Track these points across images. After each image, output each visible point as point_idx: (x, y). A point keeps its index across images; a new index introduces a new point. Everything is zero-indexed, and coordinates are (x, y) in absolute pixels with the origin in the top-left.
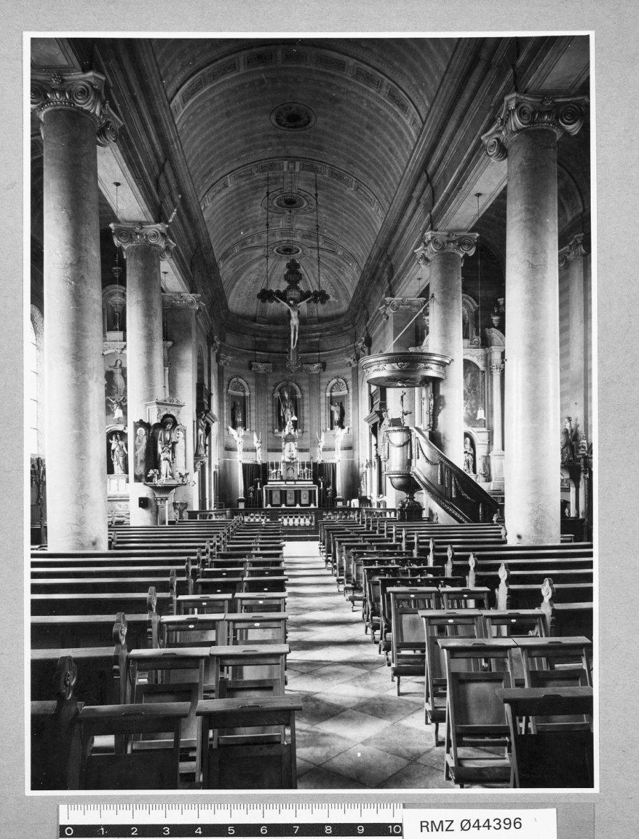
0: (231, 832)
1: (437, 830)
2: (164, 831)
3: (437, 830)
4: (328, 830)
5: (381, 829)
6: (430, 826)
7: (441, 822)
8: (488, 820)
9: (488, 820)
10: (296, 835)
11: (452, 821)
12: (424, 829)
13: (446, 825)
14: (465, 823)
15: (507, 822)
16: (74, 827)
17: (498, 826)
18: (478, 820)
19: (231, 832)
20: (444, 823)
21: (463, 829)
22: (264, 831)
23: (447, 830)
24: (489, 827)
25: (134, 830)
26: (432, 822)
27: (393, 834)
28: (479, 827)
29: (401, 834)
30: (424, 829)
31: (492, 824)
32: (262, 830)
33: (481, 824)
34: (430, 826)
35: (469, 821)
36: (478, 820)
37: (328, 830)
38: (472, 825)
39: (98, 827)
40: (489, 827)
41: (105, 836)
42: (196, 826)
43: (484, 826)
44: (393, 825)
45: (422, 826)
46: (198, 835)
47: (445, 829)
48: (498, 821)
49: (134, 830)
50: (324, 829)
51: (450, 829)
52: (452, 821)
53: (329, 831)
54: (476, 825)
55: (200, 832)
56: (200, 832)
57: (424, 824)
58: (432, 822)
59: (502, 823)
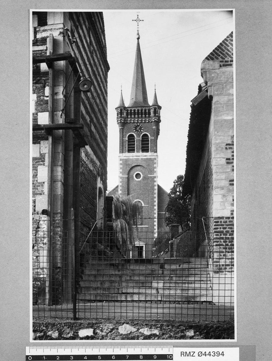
0: (100, 358)
1: (188, 356)
2: (71, 358)
3: (188, 356)
4: (141, 357)
5: (219, 354)
6: (185, 354)
7: (190, 352)
8: (210, 352)
9: (210, 352)
10: (127, 360)
11: (194, 352)
12: (182, 355)
13: (192, 354)
14: (201, 355)
15: (218, 353)
16: (32, 356)
17: (214, 355)
18: (205, 352)
19: (100, 358)
20: (191, 352)
21: (199, 356)
22: (114, 358)
23: (192, 356)
24: (210, 355)
25: (58, 357)
26: (186, 352)
27: (169, 359)
28: (206, 355)
29: (172, 359)
30: (182, 355)
31: (212, 354)
32: (156, 357)
33: (207, 354)
34: (185, 354)
35: (202, 352)
36: (205, 352)
37: (141, 357)
38: (220, 354)
39: (43, 356)
40: (210, 355)
41: (46, 360)
42: (85, 356)
43: (208, 355)
44: (169, 355)
45: (181, 354)
46: (85, 360)
47: (191, 355)
48: (214, 353)
49: (58, 357)
50: (140, 357)
51: (193, 355)
52: (194, 352)
53: (142, 358)
54: (205, 354)
55: (86, 358)
56: (86, 358)
57: (182, 353)
58: (186, 352)
59: (216, 354)
